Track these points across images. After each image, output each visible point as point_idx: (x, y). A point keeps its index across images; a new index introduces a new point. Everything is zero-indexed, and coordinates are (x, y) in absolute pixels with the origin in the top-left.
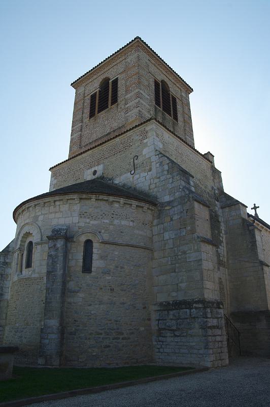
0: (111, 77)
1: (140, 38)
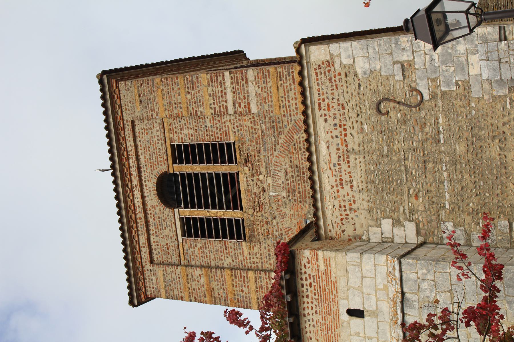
0: (164, 168)
1: (104, 72)
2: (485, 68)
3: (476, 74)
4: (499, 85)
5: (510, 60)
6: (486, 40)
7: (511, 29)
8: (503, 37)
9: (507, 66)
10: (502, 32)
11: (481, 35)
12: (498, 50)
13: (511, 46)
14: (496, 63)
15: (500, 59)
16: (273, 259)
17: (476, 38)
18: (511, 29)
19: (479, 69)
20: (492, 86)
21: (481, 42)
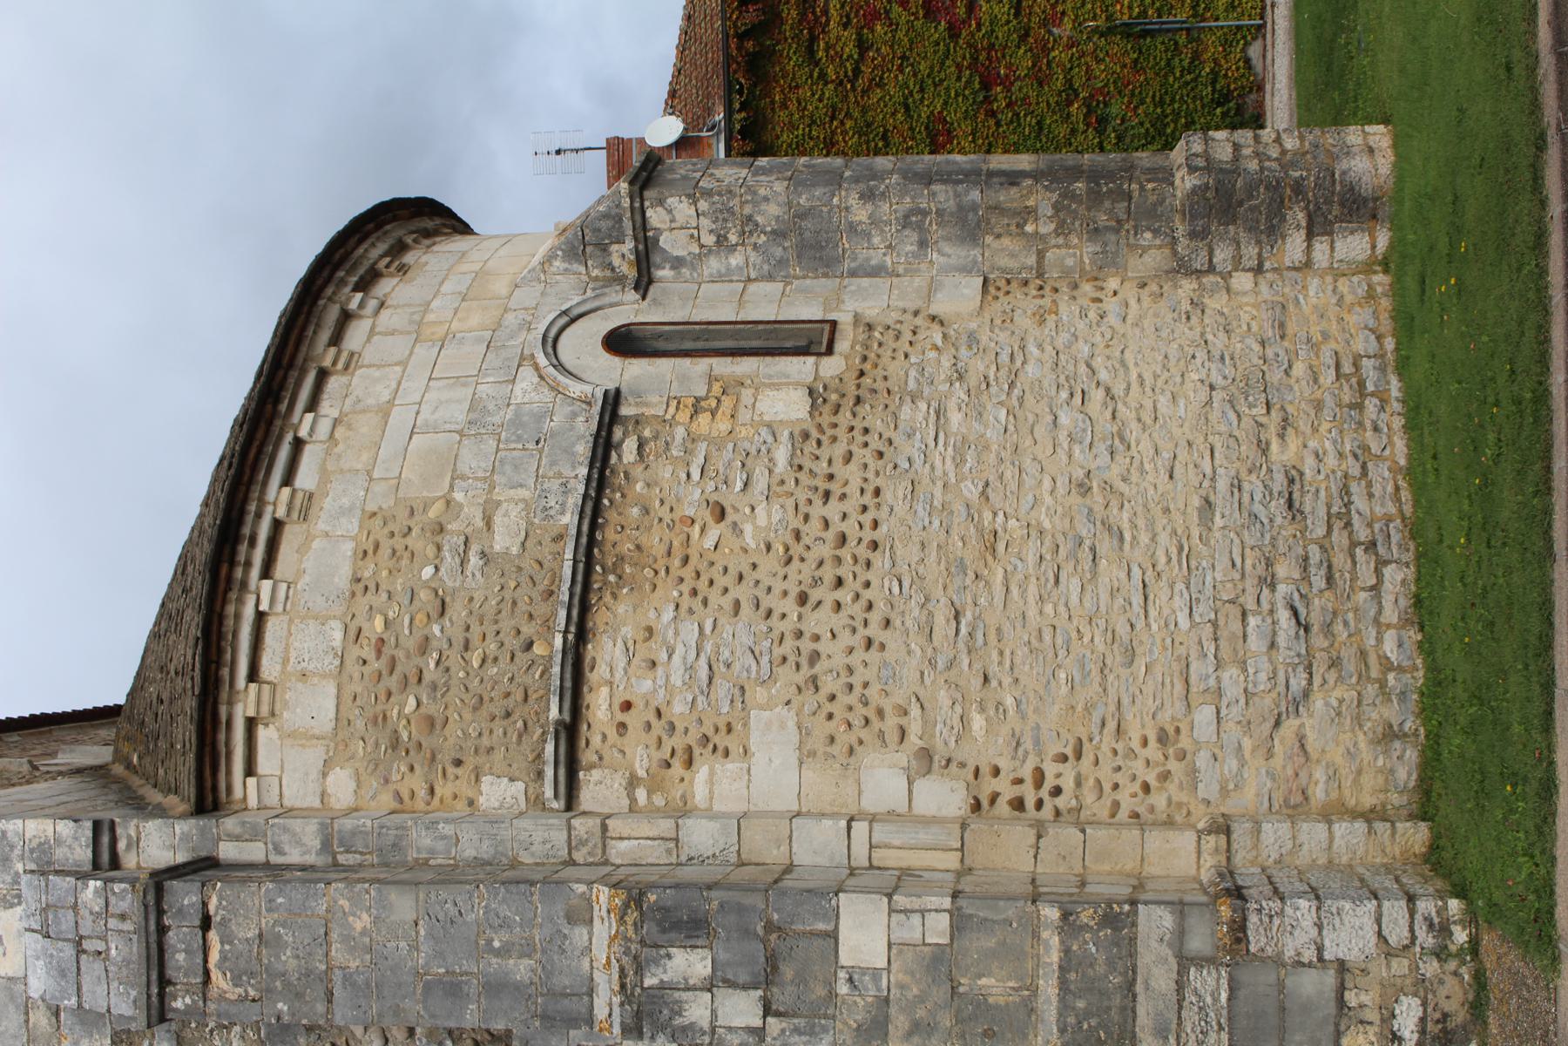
2: (38, 958)
3: (10, 974)
4: (82, 1023)
5: (108, 949)
6: (49, 863)
7: (133, 834)
8: (105, 857)
9: (98, 966)
10: (105, 839)
11: (34, 844)
12: (75, 907)
13: (113, 900)
14: (69, 951)
15: (81, 937)
16: (1357, 236)
17: (17, 852)
18: (133, 834)
19: (19, 959)
20: (58, 1021)
21: (33, 867)
